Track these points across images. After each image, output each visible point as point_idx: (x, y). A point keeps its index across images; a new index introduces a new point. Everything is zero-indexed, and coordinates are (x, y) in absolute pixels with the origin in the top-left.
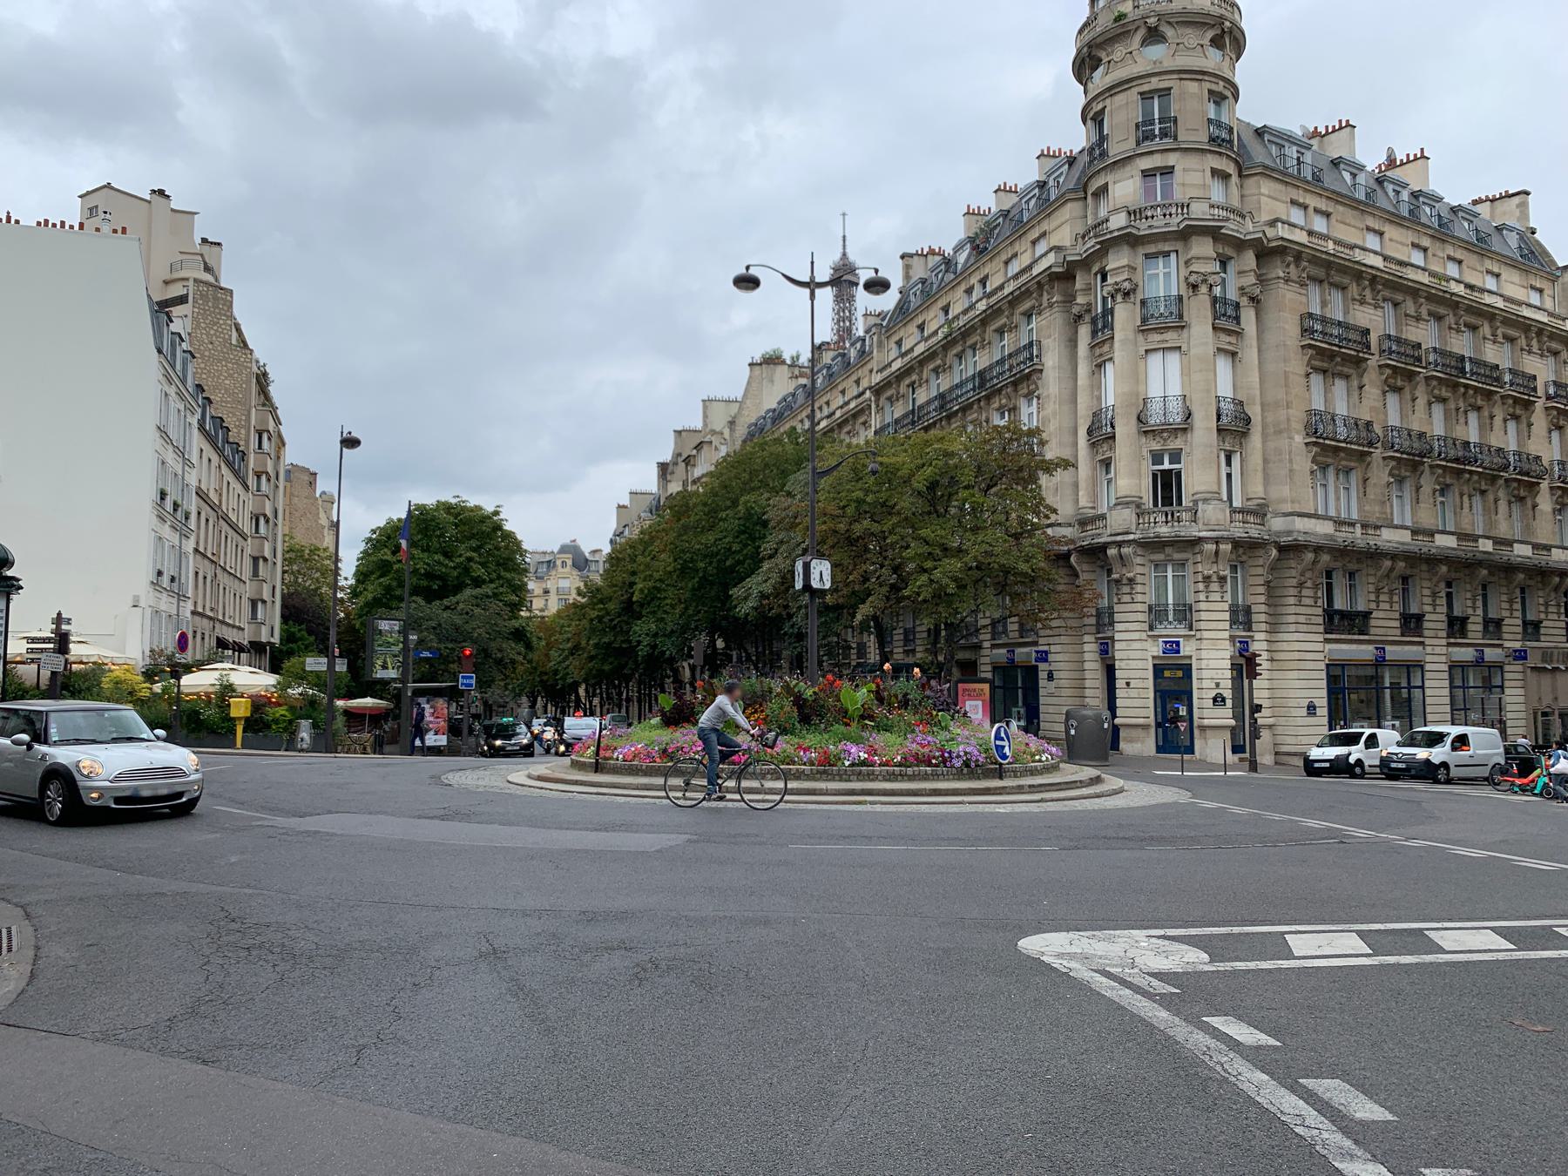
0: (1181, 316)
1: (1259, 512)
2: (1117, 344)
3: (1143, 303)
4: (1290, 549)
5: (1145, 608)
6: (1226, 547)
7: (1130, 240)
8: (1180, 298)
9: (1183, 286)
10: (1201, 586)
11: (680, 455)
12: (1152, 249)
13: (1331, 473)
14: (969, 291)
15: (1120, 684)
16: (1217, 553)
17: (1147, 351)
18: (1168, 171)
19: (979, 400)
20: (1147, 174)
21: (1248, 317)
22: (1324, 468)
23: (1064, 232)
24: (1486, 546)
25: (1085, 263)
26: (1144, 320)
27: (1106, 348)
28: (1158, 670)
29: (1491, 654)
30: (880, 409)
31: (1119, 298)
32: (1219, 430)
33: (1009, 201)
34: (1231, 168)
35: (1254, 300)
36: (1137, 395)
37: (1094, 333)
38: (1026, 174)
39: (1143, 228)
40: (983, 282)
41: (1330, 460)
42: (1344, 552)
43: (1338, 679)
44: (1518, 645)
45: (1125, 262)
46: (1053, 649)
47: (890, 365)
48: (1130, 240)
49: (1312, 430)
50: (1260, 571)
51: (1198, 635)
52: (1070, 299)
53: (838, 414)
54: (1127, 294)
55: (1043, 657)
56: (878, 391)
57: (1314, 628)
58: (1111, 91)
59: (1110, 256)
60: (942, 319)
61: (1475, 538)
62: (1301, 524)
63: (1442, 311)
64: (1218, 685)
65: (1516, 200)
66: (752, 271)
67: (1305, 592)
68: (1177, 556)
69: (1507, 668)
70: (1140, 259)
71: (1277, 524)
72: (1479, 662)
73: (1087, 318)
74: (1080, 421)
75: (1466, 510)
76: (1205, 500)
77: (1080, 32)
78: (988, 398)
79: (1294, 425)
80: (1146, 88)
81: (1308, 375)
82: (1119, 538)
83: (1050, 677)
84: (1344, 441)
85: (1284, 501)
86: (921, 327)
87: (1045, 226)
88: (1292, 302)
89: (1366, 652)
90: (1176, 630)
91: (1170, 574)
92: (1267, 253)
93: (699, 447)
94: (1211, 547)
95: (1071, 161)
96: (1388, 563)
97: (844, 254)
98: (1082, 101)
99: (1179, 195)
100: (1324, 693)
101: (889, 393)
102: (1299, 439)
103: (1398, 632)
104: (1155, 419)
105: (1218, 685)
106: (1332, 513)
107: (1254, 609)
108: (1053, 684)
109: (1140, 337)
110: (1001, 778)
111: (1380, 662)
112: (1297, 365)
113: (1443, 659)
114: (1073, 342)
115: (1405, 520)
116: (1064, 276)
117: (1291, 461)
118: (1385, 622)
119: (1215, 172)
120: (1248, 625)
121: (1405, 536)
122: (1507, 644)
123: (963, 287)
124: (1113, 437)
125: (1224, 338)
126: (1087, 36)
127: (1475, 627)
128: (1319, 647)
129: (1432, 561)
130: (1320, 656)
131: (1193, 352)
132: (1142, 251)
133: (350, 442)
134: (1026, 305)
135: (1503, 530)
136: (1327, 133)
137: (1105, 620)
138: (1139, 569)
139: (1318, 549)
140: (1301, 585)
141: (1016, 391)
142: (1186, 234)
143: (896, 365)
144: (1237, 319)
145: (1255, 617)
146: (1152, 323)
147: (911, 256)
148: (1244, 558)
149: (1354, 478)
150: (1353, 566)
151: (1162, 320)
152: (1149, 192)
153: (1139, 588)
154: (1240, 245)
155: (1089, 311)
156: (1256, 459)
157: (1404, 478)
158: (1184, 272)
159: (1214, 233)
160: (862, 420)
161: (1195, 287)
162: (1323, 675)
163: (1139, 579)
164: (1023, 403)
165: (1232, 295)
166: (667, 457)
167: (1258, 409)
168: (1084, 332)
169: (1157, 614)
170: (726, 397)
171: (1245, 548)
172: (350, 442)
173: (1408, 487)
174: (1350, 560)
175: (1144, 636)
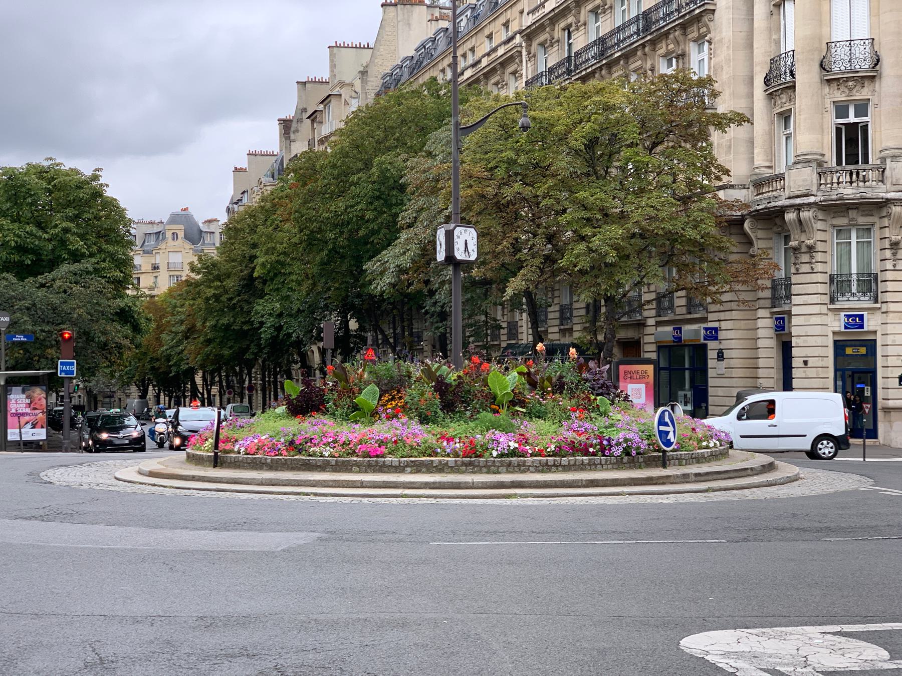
11: (304, 110)
15: (796, 362)
19: (643, 46)
28: (839, 347)
30: (532, 56)
36: (820, 40)
46: (724, 325)
51: (884, 307)
53: (485, 62)
55: (713, 333)
56: (529, 35)
68: (862, 220)
74: (757, 69)
78: (654, 43)
82: (798, 201)
83: (721, 356)
91: (854, 240)
93: (326, 100)
101: (542, 38)
108: (723, 364)
137: (781, 292)
138: (820, 236)
141: (685, 34)
160: (511, 69)
163: (820, 246)
166: (290, 112)
169: (838, 285)
175: (824, 309)
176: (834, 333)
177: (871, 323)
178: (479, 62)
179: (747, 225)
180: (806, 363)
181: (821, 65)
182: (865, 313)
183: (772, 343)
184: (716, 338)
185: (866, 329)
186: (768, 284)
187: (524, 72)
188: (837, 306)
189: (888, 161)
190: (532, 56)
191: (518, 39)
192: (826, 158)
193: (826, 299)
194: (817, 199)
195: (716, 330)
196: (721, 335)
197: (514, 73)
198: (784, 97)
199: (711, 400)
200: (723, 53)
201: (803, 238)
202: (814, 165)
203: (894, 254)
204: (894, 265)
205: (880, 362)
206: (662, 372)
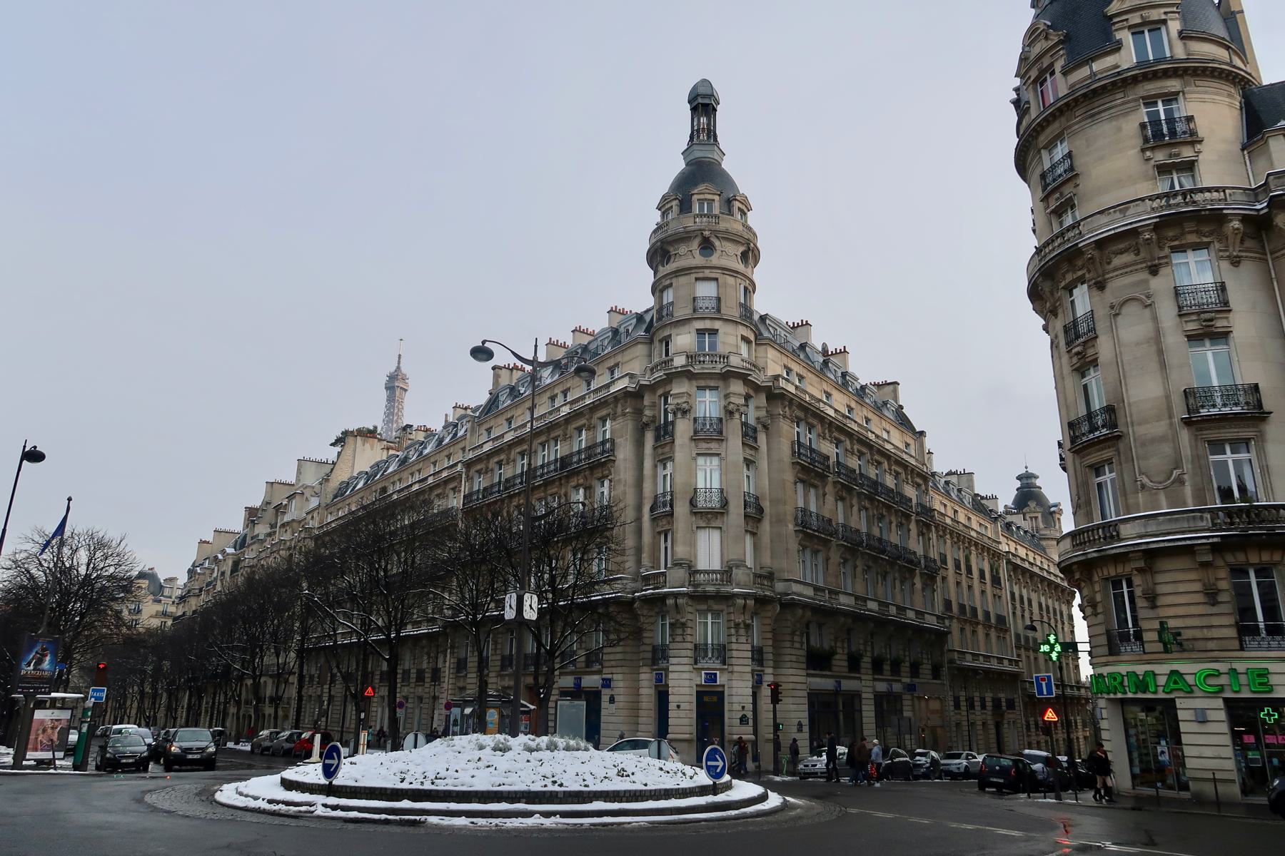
0: (721, 433)
1: (770, 576)
2: (677, 448)
3: (695, 420)
4: (788, 605)
5: (690, 646)
6: (751, 602)
7: (687, 374)
8: (720, 420)
9: (723, 412)
10: (733, 631)
11: (268, 503)
12: (702, 383)
13: (808, 553)
14: (553, 398)
15: (672, 706)
18: (714, 332)
19: (560, 479)
20: (700, 332)
21: (762, 438)
22: (804, 548)
23: (635, 366)
25: (652, 388)
26: (696, 432)
27: (667, 449)
28: (700, 695)
29: (897, 687)
30: (469, 478)
31: (679, 415)
32: (746, 516)
33: (585, 340)
34: (752, 338)
35: (765, 427)
37: (657, 438)
38: (599, 323)
39: (697, 369)
40: (565, 393)
42: (817, 610)
46: (615, 677)
47: (481, 446)
48: (687, 374)
50: (768, 621)
51: (730, 669)
53: (430, 480)
54: (685, 412)
55: (607, 683)
56: (469, 465)
62: (796, 588)
63: (864, 450)
65: (891, 387)
66: (487, 345)
67: (797, 639)
68: (716, 607)
71: (780, 587)
73: (652, 427)
77: (655, 232)
78: (568, 477)
80: (700, 275)
83: (612, 700)
86: (509, 421)
87: (619, 358)
88: (788, 431)
90: (712, 664)
91: (710, 621)
92: (774, 395)
93: (291, 498)
94: (740, 602)
95: (640, 318)
97: (398, 368)
99: (721, 349)
101: (479, 467)
102: (791, 527)
104: (701, 503)
108: (613, 706)
109: (693, 444)
110: (715, 794)
112: (789, 476)
113: (804, 687)
114: (639, 444)
115: (853, 591)
116: (635, 395)
118: (840, 662)
119: (744, 339)
123: (548, 394)
125: (748, 451)
126: (660, 236)
128: (802, 679)
130: (804, 687)
132: (695, 383)
133: (33, 456)
134: (603, 412)
137: (659, 656)
138: (690, 616)
140: (793, 633)
141: (592, 474)
142: (727, 376)
143: (487, 448)
144: (755, 439)
145: (765, 656)
146: (702, 435)
147: (500, 368)
149: (821, 557)
152: (701, 345)
153: (689, 631)
154: (757, 388)
155: (653, 421)
158: (723, 403)
159: (744, 378)
160: (452, 485)
161: (731, 413)
162: (806, 701)
163: (689, 624)
164: (596, 484)
165: (752, 421)
166: (257, 503)
168: (649, 438)
170: (318, 459)
171: (761, 601)
172: (33, 456)
173: (849, 566)
174: (823, 614)
180: (678, 707)
181: (691, 502)
183: (652, 691)
184: (609, 686)
186: (650, 648)
188: (699, 666)
190: (469, 478)
191: (459, 467)
193: (692, 661)
195: (610, 680)
197: (454, 489)
198: (664, 521)
199: (602, 732)
201: (678, 617)
205: (726, 708)
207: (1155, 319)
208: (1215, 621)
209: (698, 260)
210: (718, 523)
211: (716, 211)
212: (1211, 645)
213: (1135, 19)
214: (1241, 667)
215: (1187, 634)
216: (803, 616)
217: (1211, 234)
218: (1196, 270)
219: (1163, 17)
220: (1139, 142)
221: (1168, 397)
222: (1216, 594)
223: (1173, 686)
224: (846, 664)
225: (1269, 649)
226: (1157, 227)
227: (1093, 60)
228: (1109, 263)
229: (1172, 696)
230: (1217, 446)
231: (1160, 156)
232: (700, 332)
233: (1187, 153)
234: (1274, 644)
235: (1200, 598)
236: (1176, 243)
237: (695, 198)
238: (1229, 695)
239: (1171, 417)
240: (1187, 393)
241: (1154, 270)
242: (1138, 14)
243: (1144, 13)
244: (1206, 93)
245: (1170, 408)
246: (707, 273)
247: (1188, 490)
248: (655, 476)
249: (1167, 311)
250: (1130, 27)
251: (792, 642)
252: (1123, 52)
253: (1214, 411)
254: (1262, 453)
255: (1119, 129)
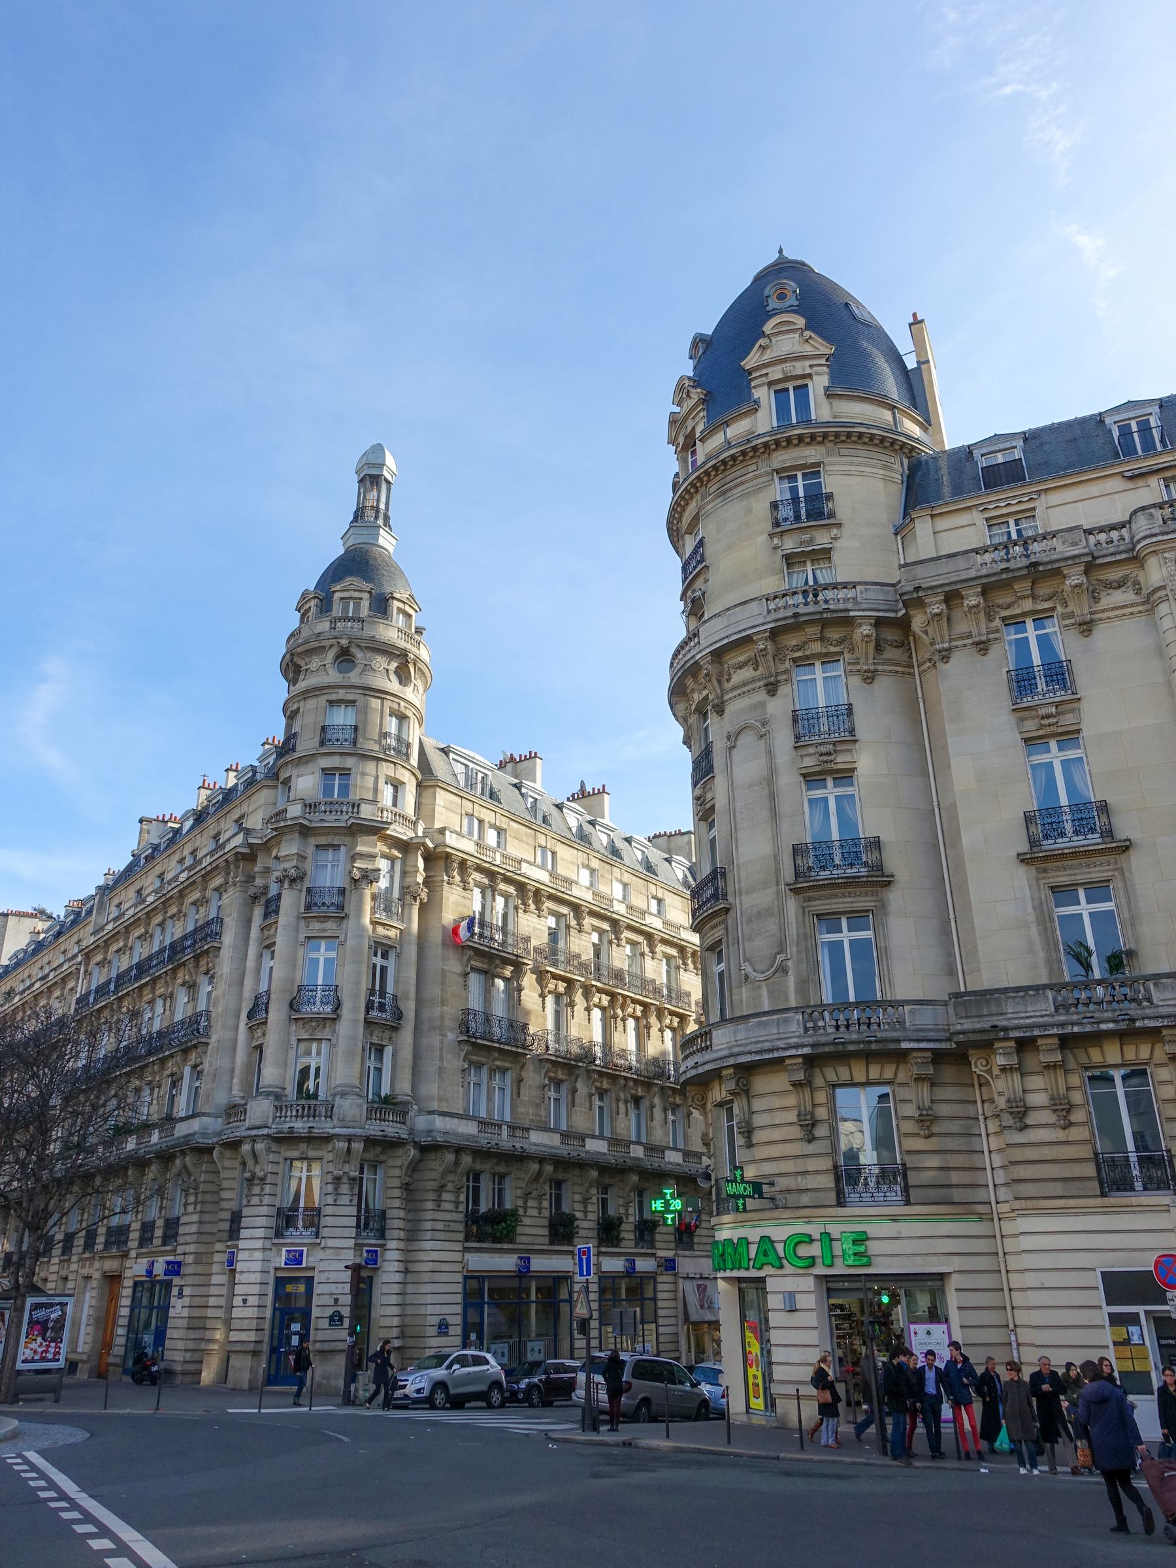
0: (341, 907)
3: (309, 891)
4: (429, 1149)
6: (358, 1146)
7: (305, 831)
16: (349, 1150)
17: (309, 938)
20: (327, 772)
24: (638, 1152)
26: (308, 908)
28: (280, 1282)
29: (644, 1265)
32: (367, 1022)
36: (293, 982)
39: (315, 820)
41: (483, 1059)
43: (476, 1290)
44: (670, 1254)
45: (294, 850)
47: (102, 928)
49: (464, 1027)
50: (397, 1172)
52: (250, 878)
54: (293, 881)
57: (453, 1236)
58: (307, 694)
59: (283, 844)
60: (158, 884)
61: (627, 1144)
62: (440, 1123)
64: (336, 1300)
69: (660, 1279)
70: (311, 850)
72: (630, 1272)
74: (244, 1004)
75: (622, 1115)
76: (343, 1095)
79: (447, 1023)
80: (334, 697)
81: (466, 975)
82: (254, 1132)
84: (499, 1042)
85: (432, 1099)
89: (506, 1262)
94: (343, 1145)
96: (535, 1167)
98: (286, 696)
100: (459, 1309)
103: (546, 1240)
105: (336, 1300)
106: (483, 1114)
107: (389, 1214)
109: (302, 924)
111: (524, 1272)
113: (458, 1267)
114: (248, 922)
117: (441, 1058)
118: (533, 1226)
120: (382, 1233)
121: (554, 1140)
122: (661, 1253)
124: (265, 1023)
127: (628, 1233)
129: (581, 1164)
130: (458, 1267)
131: (349, 943)
132: (313, 841)
135: (659, 1135)
136: (521, 761)
139: (459, 1150)
140: (441, 1188)
145: (390, 1224)
147: (150, 821)
148: (382, 1158)
150: (501, 1169)
151: (324, 909)
152: (328, 790)
155: (265, 893)
156: (406, 1055)
157: (562, 1081)
167: (412, 1005)
168: (258, 912)
169: (286, 1219)
176: (276, 1269)
177: (311, 1259)
178: (48, 975)
179: (215, 1153)
180: (245, 1301)
181: (291, 1006)
182: (305, 1249)
184: (178, 1273)
185: (304, 1265)
187: (79, 989)
189: (337, 1098)
192: (287, 1092)
194: (271, 1132)
195: (179, 1264)
196: (184, 1270)
200: (222, 987)
202: (272, 1098)
203: (336, 1189)
204: (335, 1200)
206: (567, 1297)
207: (770, 753)
208: (812, 1165)
209: (333, 676)
210: (326, 1033)
211: (364, 611)
212: (805, 1199)
213: (776, 373)
214: (835, 1229)
215: (782, 1183)
216: (457, 1163)
217: (840, 642)
218: (822, 686)
219: (808, 371)
220: (768, 526)
221: (776, 856)
222: (1025, 1114)
223: (763, 1259)
224: (546, 1231)
225: (874, 1202)
226: (774, 634)
227: (727, 424)
228: (728, 680)
229: (761, 1274)
230: (830, 920)
231: (790, 544)
232: (327, 772)
233: (822, 539)
234: (879, 1196)
235: (796, 1132)
236: (799, 654)
237: (337, 596)
238: (820, 1270)
239: (778, 884)
240: (798, 851)
241: (772, 689)
242: (779, 367)
243: (787, 366)
244: (852, 464)
245: (777, 871)
246: (342, 694)
247: (791, 981)
248: (258, 969)
249: (783, 738)
250: (770, 384)
251: (439, 1201)
252: (760, 413)
253: (1062, 843)
254: (880, 929)
255: (749, 510)
